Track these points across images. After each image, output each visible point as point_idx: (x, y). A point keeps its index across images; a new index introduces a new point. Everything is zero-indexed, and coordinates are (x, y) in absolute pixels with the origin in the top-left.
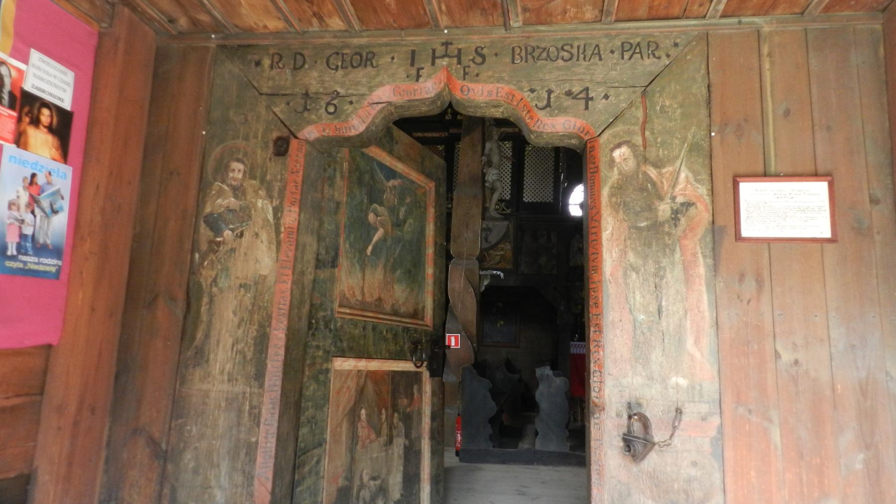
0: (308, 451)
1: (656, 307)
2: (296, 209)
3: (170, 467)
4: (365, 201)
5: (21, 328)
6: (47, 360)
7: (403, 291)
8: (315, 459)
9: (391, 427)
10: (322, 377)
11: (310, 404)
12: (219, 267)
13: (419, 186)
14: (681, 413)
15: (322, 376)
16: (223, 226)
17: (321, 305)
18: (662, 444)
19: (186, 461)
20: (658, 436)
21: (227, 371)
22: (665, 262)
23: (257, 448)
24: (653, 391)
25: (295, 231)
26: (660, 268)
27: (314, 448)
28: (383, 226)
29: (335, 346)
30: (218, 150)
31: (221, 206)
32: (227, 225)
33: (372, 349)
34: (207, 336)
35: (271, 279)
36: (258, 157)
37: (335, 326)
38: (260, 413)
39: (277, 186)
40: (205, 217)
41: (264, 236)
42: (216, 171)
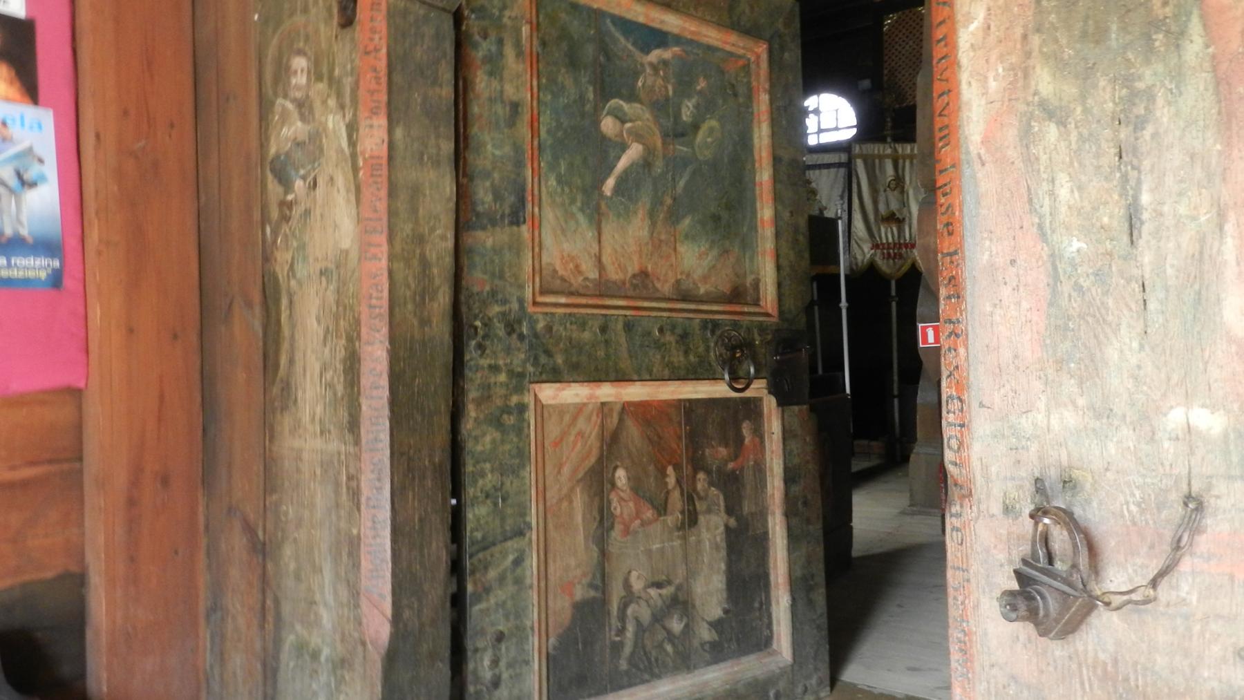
0: (494, 544)
1: (1120, 212)
2: (382, 121)
3: (270, 566)
4: (591, 96)
5: (22, 370)
6: (80, 408)
7: (701, 256)
8: (511, 558)
9: (690, 498)
10: (510, 420)
11: (488, 466)
12: (295, 244)
13: (731, 54)
14: (1200, 507)
15: (510, 418)
16: (293, 173)
17: (493, 293)
18: (1117, 600)
19: (286, 560)
20: (1117, 577)
21: (317, 418)
22: (1148, 76)
23: (359, 545)
24: (1112, 448)
25: (384, 161)
26: (1134, 95)
27: (505, 540)
28: (638, 138)
29: (536, 362)
30: (275, 41)
31: (287, 139)
32: (297, 170)
33: (625, 364)
34: (291, 361)
35: (354, 255)
36: (323, 38)
37: (532, 327)
38: (358, 486)
39: (348, 82)
40: (272, 162)
41: (340, 181)
42: (277, 80)
